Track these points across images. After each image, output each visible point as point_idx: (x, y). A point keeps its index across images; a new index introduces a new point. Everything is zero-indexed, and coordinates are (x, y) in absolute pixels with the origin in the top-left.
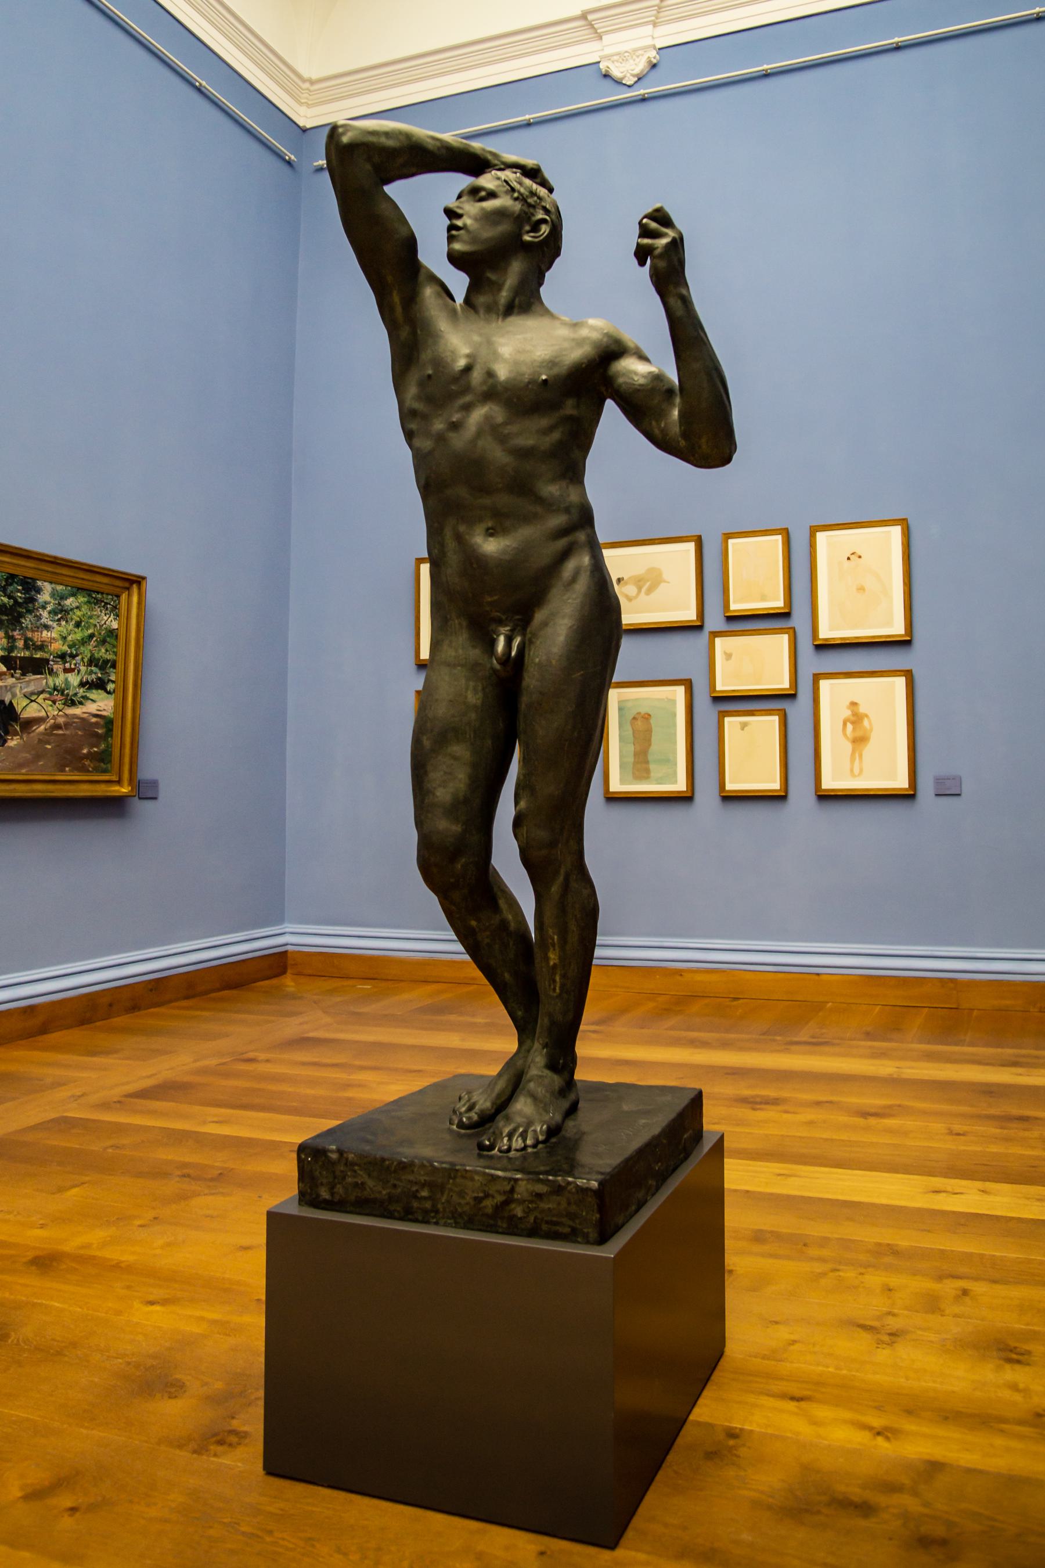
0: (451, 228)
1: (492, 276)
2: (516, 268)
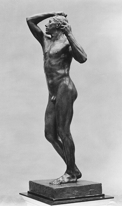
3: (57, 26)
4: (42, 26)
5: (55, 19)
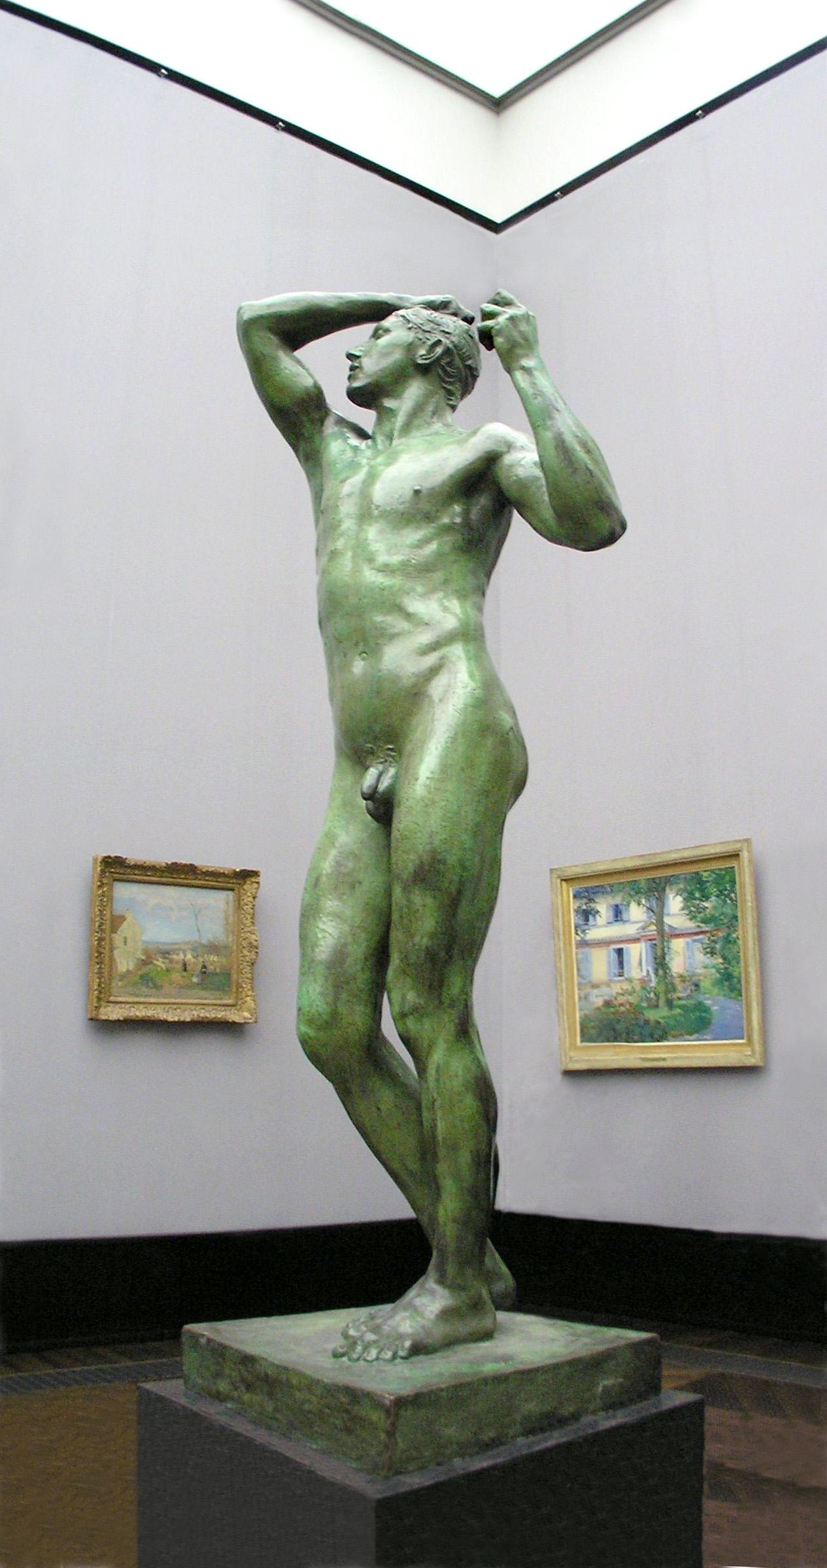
0: (352, 369)
1: (388, 403)
2: (414, 390)
3: (423, 352)
5: (411, 318)
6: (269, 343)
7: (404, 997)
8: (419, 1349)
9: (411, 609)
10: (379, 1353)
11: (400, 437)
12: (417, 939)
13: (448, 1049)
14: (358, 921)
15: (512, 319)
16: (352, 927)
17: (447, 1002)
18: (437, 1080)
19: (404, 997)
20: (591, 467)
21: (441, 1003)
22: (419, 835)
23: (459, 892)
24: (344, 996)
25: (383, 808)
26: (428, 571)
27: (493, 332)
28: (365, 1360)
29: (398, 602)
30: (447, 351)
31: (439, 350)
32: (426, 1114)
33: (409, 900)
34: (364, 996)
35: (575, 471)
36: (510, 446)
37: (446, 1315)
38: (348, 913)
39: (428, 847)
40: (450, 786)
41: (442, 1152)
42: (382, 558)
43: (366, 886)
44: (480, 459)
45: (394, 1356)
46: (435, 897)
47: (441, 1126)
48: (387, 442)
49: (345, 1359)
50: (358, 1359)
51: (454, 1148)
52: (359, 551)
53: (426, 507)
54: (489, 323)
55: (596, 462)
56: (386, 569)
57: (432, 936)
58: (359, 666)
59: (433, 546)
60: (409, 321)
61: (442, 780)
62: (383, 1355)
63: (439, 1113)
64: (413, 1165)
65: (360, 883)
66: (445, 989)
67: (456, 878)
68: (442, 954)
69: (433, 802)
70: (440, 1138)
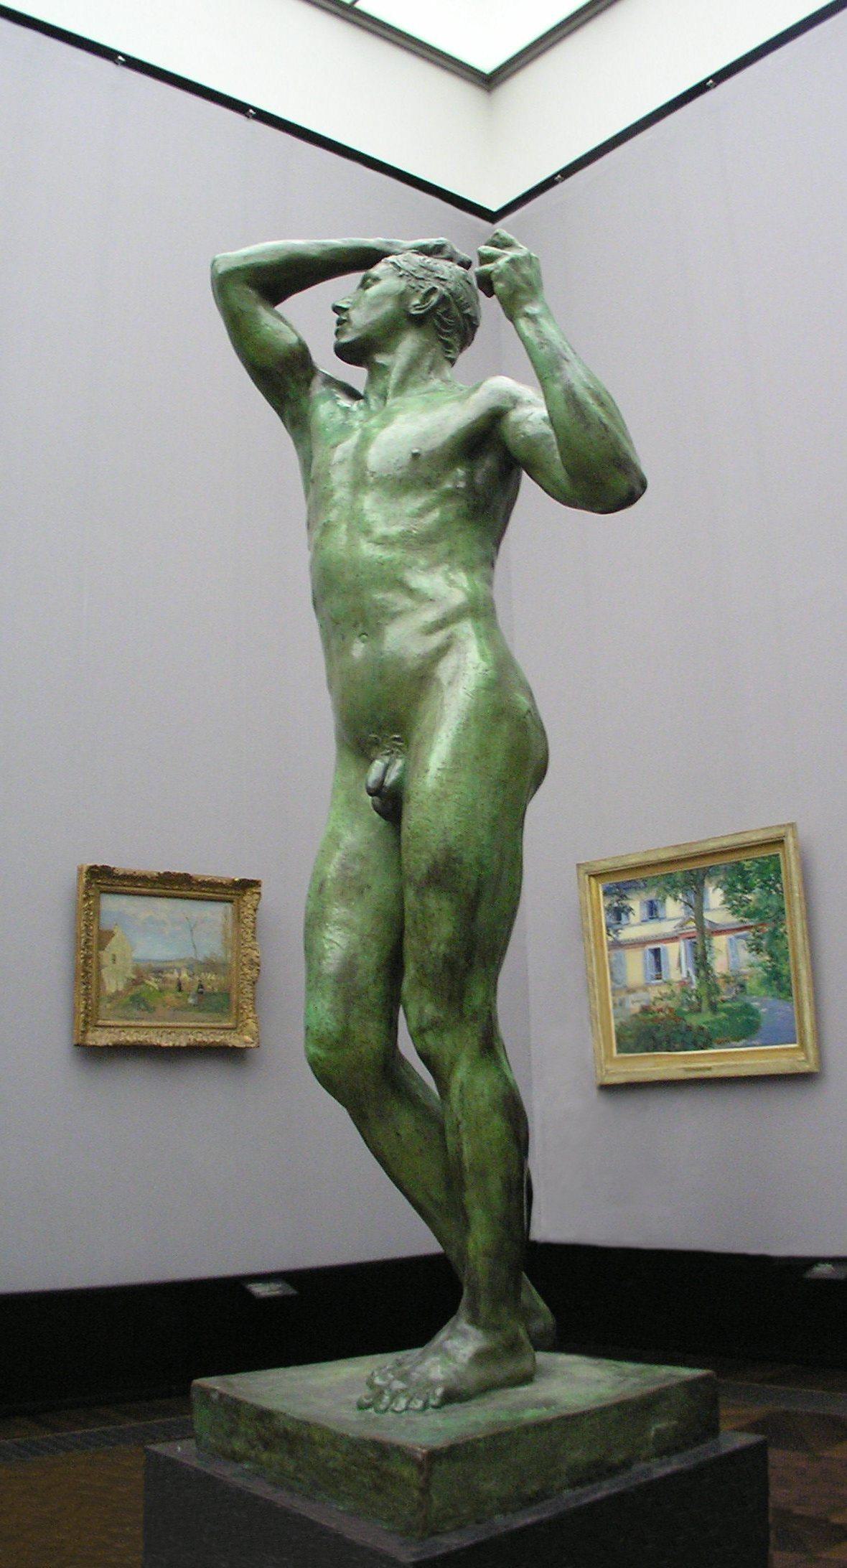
0: (340, 322)
1: (381, 359)
2: (408, 344)
3: (417, 302)
4: (307, 319)
6: (247, 298)
7: (421, 1011)
8: (452, 1397)
9: (413, 585)
10: (408, 1402)
11: (395, 395)
12: (434, 946)
13: (472, 1066)
14: (368, 929)
15: (513, 261)
16: (362, 935)
17: (469, 1013)
18: (461, 1101)
19: (421, 1011)
20: (606, 421)
21: (462, 1015)
22: (432, 832)
23: (478, 893)
24: (356, 1012)
25: (390, 803)
26: (431, 542)
27: (493, 277)
28: (394, 1411)
29: (399, 577)
30: (443, 300)
31: (434, 299)
32: (450, 1139)
33: (422, 904)
34: (377, 1011)
35: (588, 426)
36: (516, 401)
37: (480, 1358)
38: (357, 920)
39: (442, 845)
40: (463, 777)
41: (469, 1179)
42: (380, 530)
43: (376, 889)
44: (483, 417)
45: (425, 1406)
46: (451, 900)
47: (467, 1150)
48: (381, 402)
49: (371, 1410)
50: (386, 1410)
51: (483, 1174)
52: (354, 523)
53: (425, 471)
54: (488, 267)
55: (611, 416)
56: (385, 541)
57: (450, 942)
58: (358, 649)
59: (435, 515)
60: (400, 268)
61: (455, 771)
62: (412, 1405)
63: (465, 1137)
64: (438, 1194)
65: (369, 887)
66: (466, 1000)
67: (474, 878)
68: (462, 962)
69: (446, 795)
70: (467, 1165)
